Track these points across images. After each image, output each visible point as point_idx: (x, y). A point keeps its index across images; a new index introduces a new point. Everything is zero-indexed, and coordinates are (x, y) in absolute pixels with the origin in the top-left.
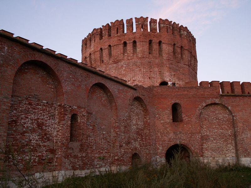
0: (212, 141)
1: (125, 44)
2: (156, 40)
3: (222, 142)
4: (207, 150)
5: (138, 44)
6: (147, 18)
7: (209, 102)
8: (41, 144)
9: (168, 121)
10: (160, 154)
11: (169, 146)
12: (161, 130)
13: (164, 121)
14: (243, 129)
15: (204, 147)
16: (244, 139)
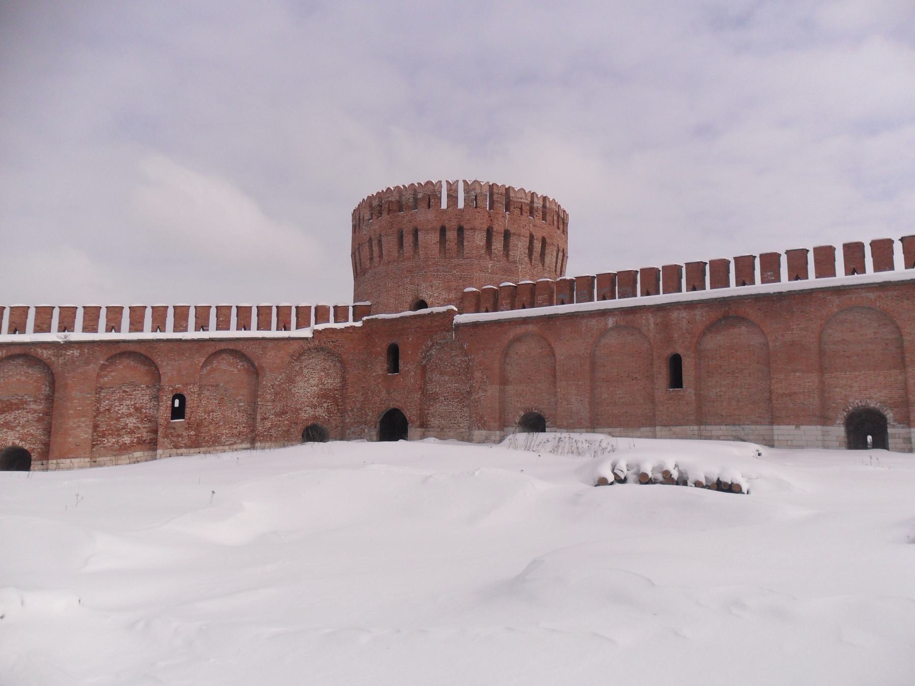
4: (433, 416)
5: (383, 239)
9: (381, 372)
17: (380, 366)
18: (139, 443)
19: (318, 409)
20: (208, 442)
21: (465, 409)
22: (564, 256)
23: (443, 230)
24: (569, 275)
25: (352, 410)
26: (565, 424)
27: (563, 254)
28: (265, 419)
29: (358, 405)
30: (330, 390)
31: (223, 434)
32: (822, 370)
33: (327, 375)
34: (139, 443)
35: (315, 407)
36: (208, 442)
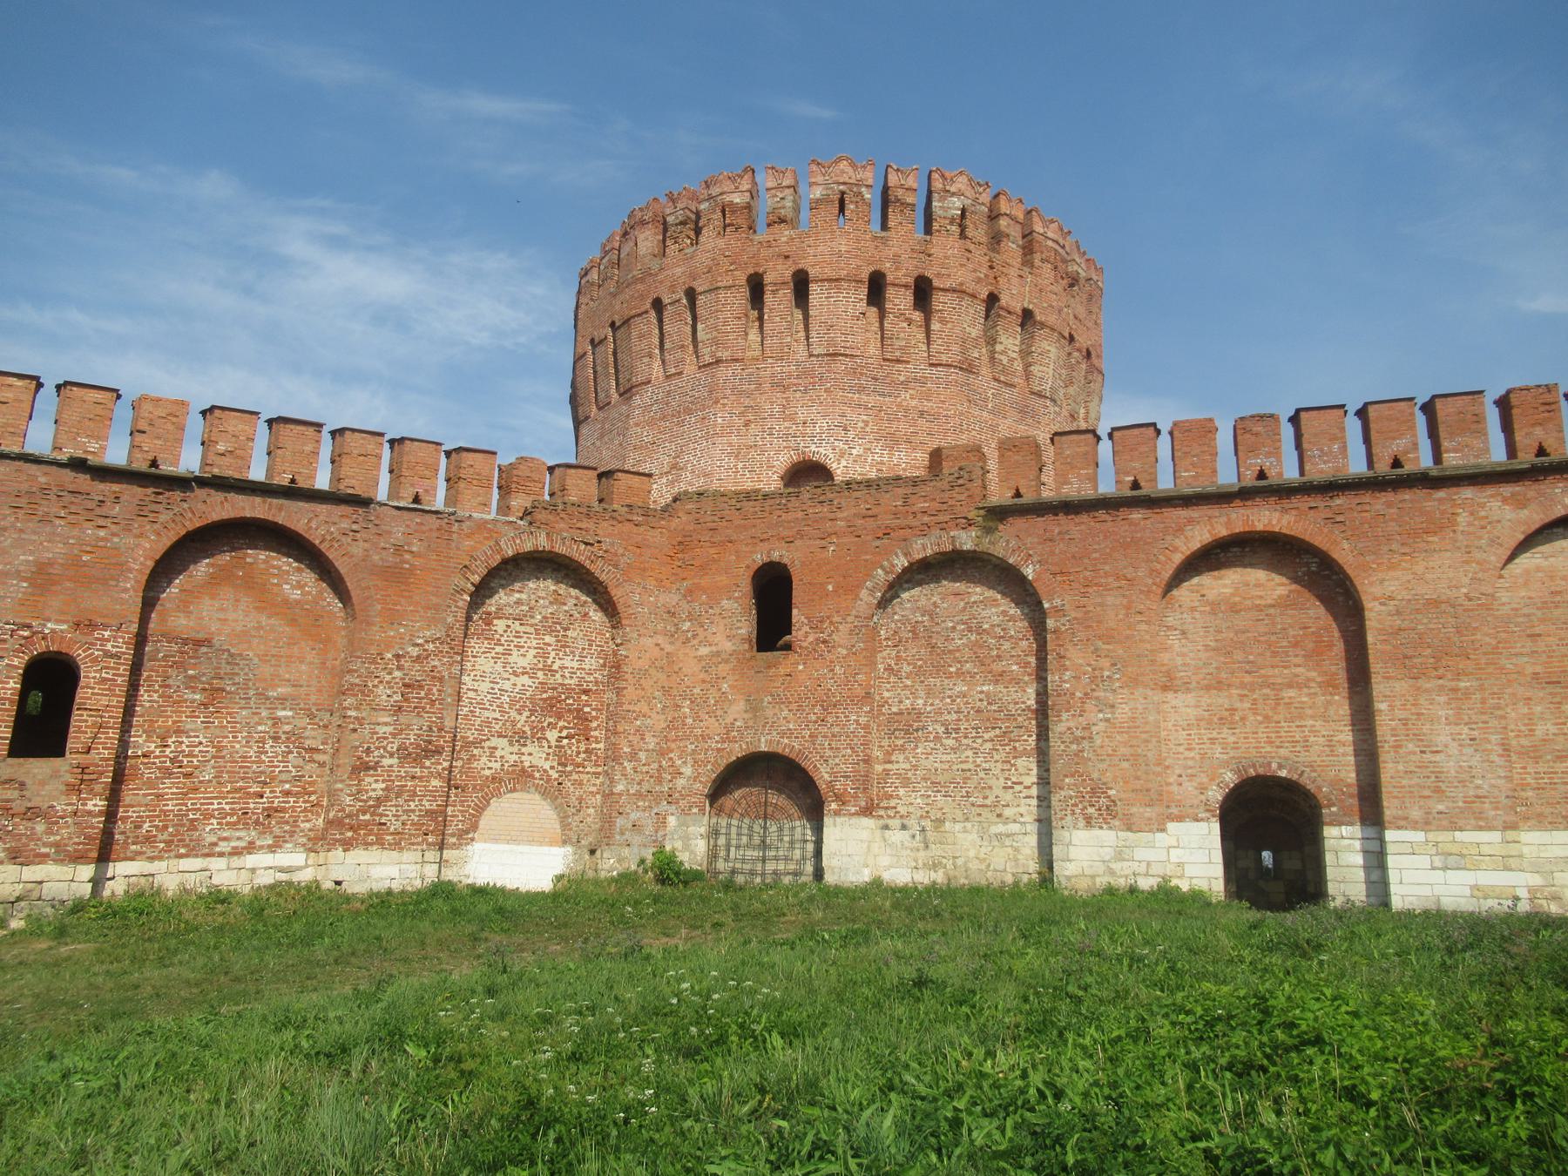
0: (937, 738)
1: (756, 288)
3: (989, 745)
4: (906, 782)
7: (924, 547)
11: (723, 763)
13: (714, 649)
14: (1093, 679)
15: (896, 766)
16: (1094, 729)
17: (735, 618)
20: (149, 839)
25: (633, 756)
26: (1416, 814)
28: (367, 767)
29: (651, 742)
30: (569, 690)
31: (208, 816)
32: (765, 818)
33: (563, 645)
35: (519, 738)
36: (149, 839)
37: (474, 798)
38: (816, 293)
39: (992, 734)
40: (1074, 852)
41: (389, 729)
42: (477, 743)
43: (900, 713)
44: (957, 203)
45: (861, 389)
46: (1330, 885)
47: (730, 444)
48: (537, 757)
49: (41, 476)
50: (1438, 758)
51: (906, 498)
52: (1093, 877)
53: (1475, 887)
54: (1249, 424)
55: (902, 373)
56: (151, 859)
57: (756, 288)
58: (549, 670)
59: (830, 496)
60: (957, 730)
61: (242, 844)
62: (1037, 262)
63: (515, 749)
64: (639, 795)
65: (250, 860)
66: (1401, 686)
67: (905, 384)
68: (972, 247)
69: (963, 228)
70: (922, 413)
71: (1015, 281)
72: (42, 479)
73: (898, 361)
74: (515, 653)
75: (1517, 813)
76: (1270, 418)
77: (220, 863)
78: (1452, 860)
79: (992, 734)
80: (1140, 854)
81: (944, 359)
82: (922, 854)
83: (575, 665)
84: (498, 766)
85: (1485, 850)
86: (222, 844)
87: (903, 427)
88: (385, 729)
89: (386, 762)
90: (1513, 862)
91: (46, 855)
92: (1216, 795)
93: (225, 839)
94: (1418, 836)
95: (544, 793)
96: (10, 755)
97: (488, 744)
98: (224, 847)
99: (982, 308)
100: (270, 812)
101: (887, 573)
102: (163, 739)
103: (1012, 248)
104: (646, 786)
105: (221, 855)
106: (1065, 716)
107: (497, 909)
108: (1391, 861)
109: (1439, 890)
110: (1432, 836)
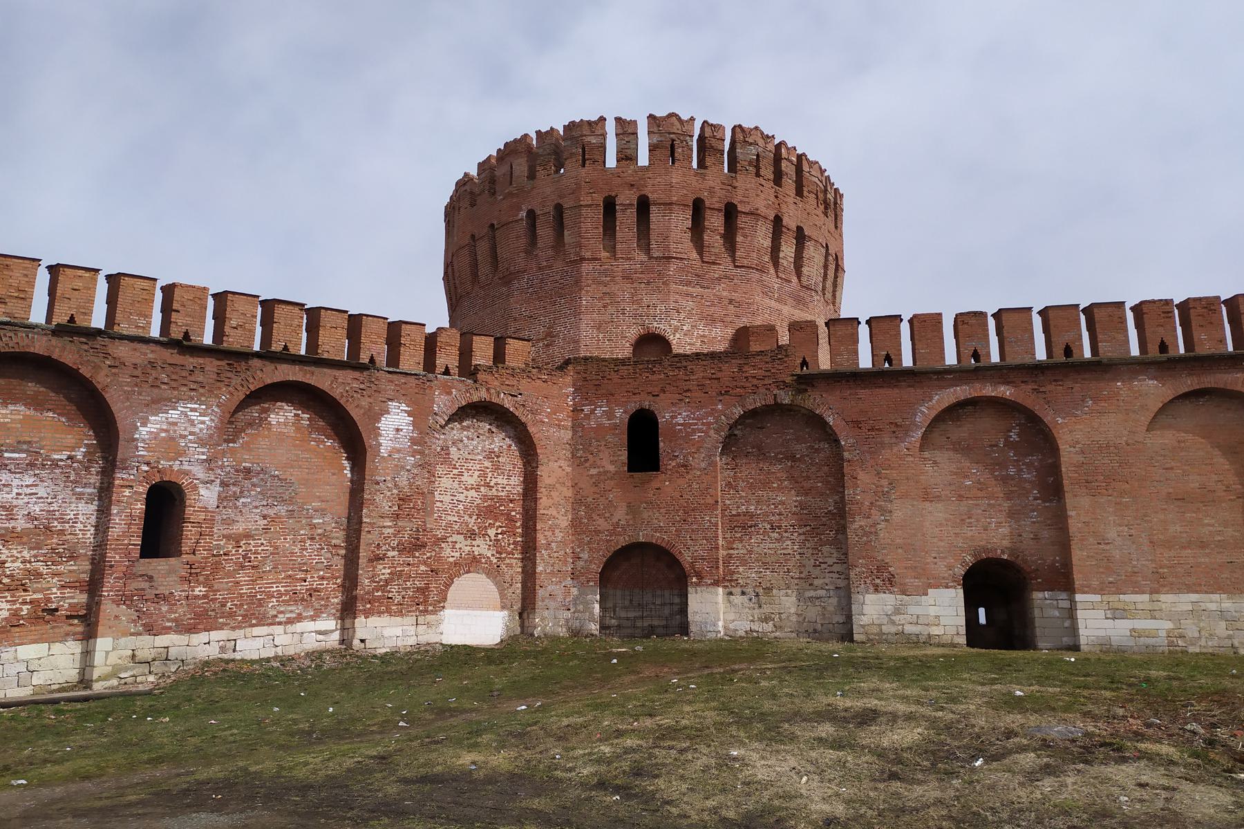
2: (626, 198)
3: (802, 537)
4: (744, 562)
6: (602, 119)
8: (43, 569)
10: (583, 574)
12: (589, 499)
17: (613, 457)
18: (35, 619)
19: (478, 541)
20: (231, 615)
21: (826, 549)
22: (839, 268)
23: (698, 208)
24: (430, 309)
26: (1095, 583)
27: (834, 266)
33: (497, 468)
34: (35, 619)
35: (471, 535)
36: (231, 615)
37: (444, 577)
38: (655, 215)
39: (804, 530)
40: (866, 609)
41: (391, 531)
42: (444, 539)
43: (739, 515)
44: (753, 150)
45: (688, 283)
46: (1037, 630)
47: (593, 320)
48: (482, 548)
49: (150, 353)
50: (1107, 547)
51: (740, 367)
52: (880, 625)
53: (1133, 630)
54: (966, 319)
55: (717, 271)
56: (233, 629)
57: (610, 207)
58: (488, 485)
59: (684, 364)
60: (780, 527)
61: (294, 615)
62: (805, 193)
63: (469, 542)
64: (552, 573)
65: (299, 627)
66: (1085, 501)
67: (719, 279)
68: (763, 182)
69: (758, 168)
70: (731, 301)
71: (792, 207)
72: (150, 356)
73: (714, 263)
74: (466, 474)
75: (1159, 583)
76: (981, 315)
77: (278, 629)
78: (1117, 613)
79: (804, 530)
80: (913, 610)
81: (745, 262)
82: (757, 611)
83: (505, 482)
84: (458, 554)
85: (1140, 606)
86: (281, 616)
87: (718, 311)
88: (389, 530)
89: (390, 554)
90: (1157, 614)
91: (170, 628)
92: (960, 571)
93: (282, 612)
94: (1097, 598)
95: (488, 574)
96: (141, 557)
97: (450, 539)
98: (281, 618)
99: (770, 227)
100: (312, 592)
101: (727, 418)
102: (238, 542)
103: (789, 184)
104: (557, 568)
105: (280, 623)
106: (857, 518)
107: (461, 657)
108: (1080, 614)
109: (1109, 633)
110: (1105, 597)
